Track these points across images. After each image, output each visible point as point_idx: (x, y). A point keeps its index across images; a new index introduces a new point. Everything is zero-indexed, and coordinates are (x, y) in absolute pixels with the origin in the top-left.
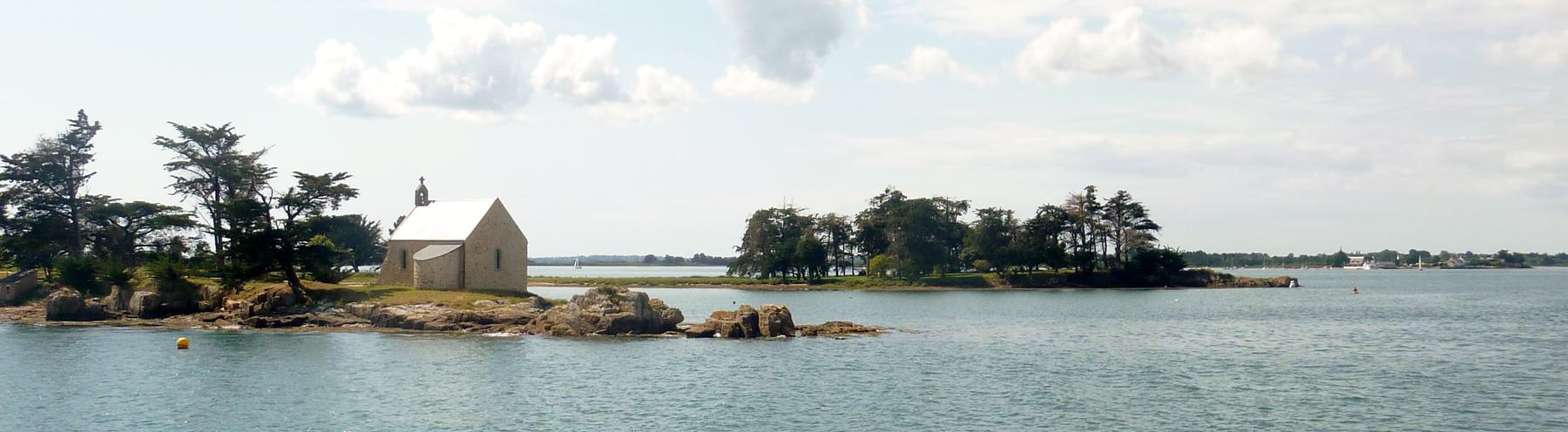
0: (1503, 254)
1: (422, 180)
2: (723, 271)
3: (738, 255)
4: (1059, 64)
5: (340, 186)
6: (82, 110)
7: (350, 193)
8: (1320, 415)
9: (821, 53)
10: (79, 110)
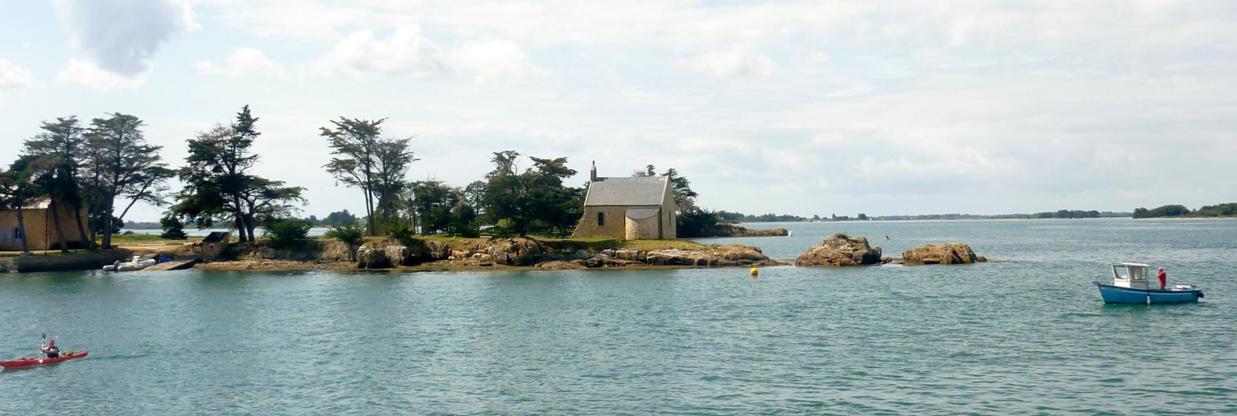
0: (1206, 208)
1: (594, 163)
2: (482, 234)
4: (360, 66)
9: (152, 49)
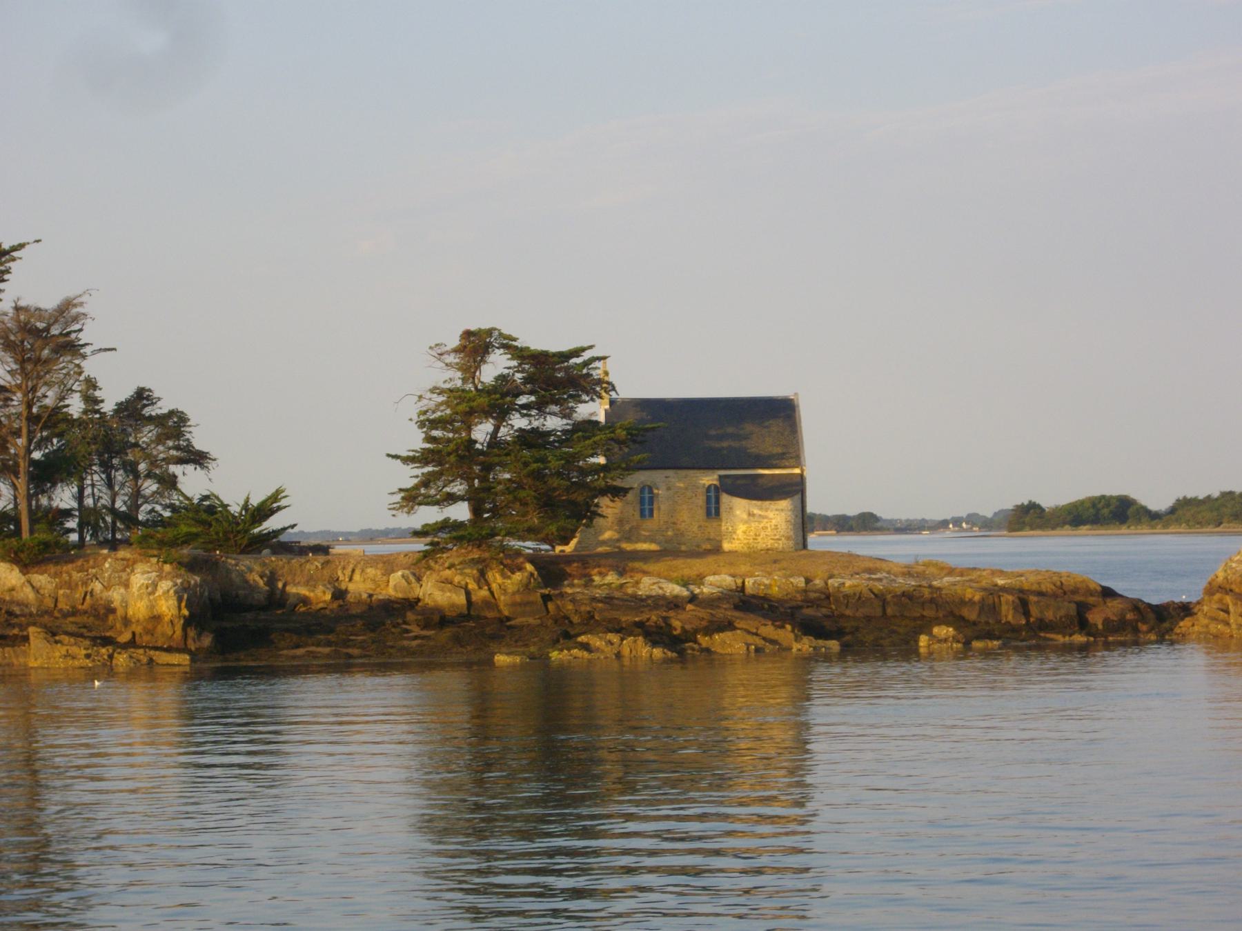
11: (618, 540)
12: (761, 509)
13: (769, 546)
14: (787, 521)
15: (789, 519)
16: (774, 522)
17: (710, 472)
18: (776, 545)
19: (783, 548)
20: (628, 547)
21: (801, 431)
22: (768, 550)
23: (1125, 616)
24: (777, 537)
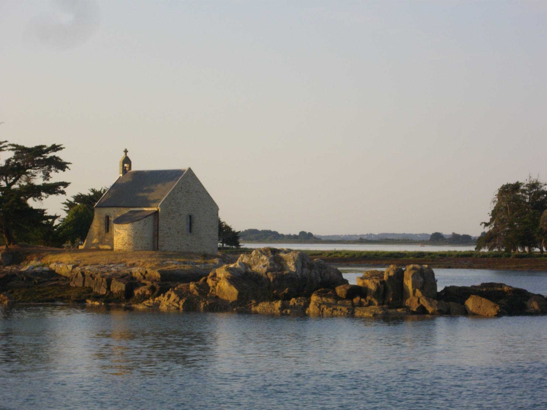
1: (126, 151)
3: (487, 230)
5: (52, 158)
6: (126, 149)
7: (62, 166)
8: (306, 391)
10: (124, 150)
11: (98, 244)
12: (118, 229)
13: (120, 248)
14: (128, 235)
15: (130, 234)
16: (122, 236)
17: (128, 208)
18: (123, 248)
19: (126, 249)
20: (101, 247)
21: (331, 236)
22: (119, 250)
23: (270, 303)
24: (123, 243)
